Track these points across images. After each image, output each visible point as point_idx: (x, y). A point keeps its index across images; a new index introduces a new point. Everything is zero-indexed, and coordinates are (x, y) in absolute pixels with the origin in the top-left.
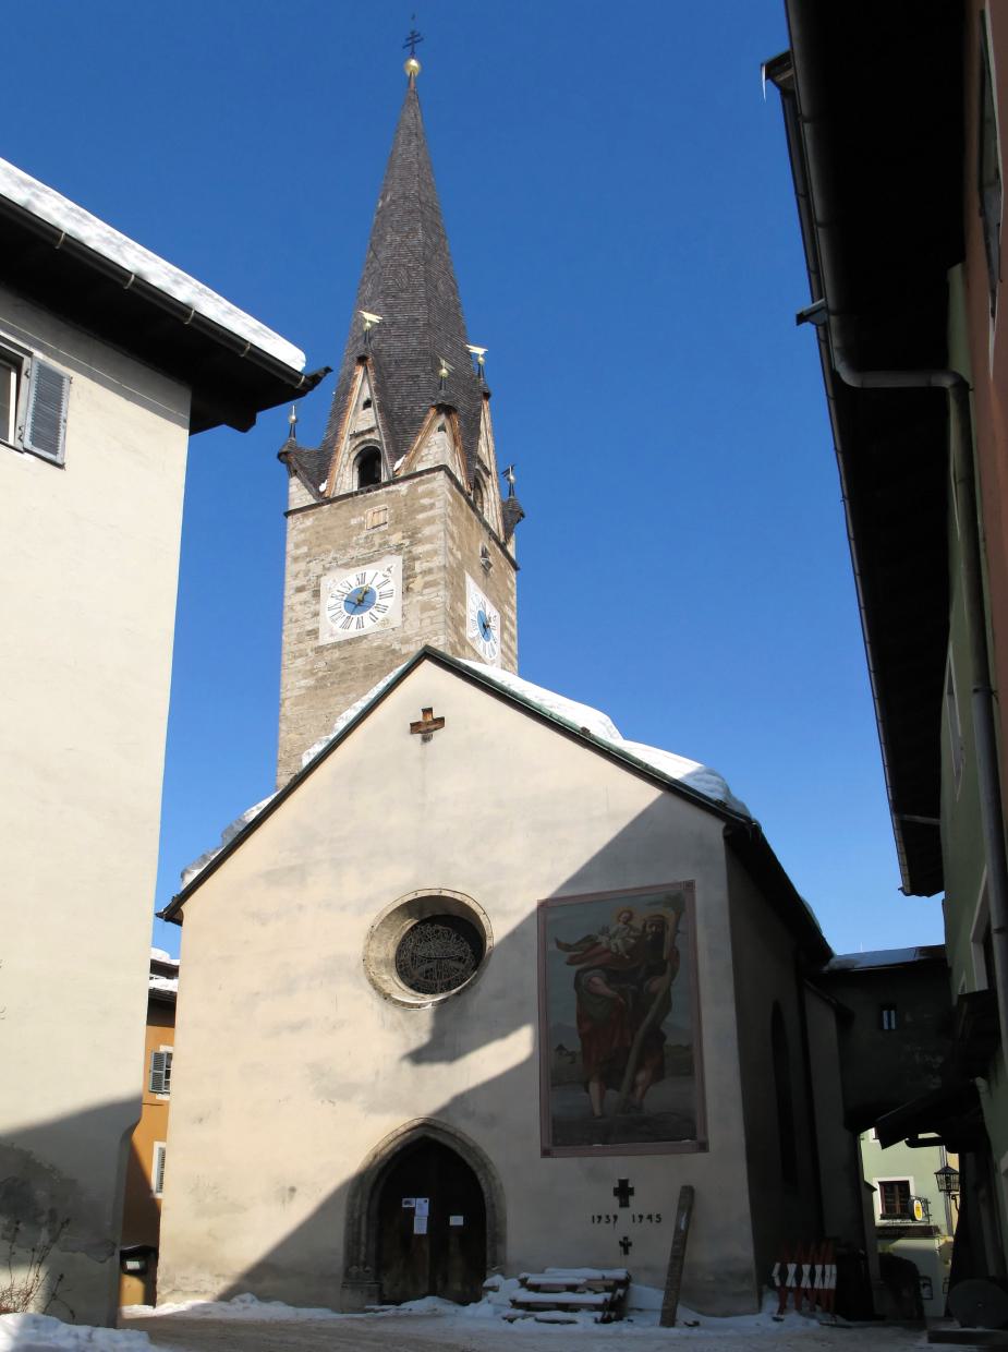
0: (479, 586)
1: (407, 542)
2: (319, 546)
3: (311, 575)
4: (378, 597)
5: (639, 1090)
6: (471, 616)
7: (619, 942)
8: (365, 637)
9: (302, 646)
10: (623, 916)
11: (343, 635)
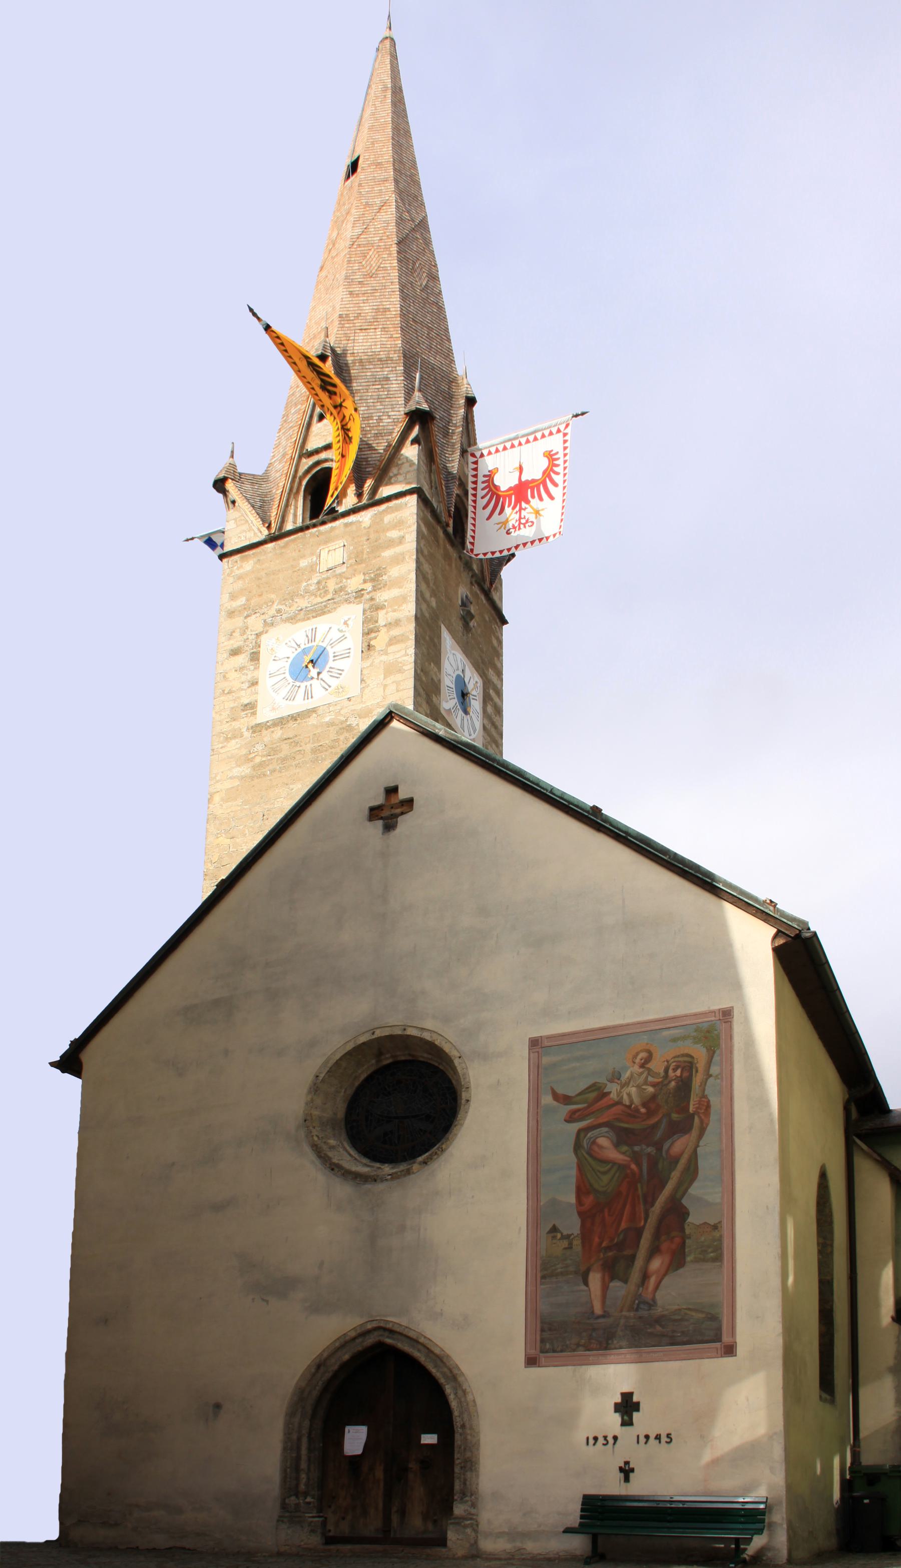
0: (458, 643)
1: (369, 587)
2: (260, 595)
3: (249, 632)
4: (331, 658)
5: (653, 1281)
6: (448, 682)
7: (633, 1090)
8: (314, 710)
9: (236, 725)
10: (640, 1057)
11: (287, 709)
